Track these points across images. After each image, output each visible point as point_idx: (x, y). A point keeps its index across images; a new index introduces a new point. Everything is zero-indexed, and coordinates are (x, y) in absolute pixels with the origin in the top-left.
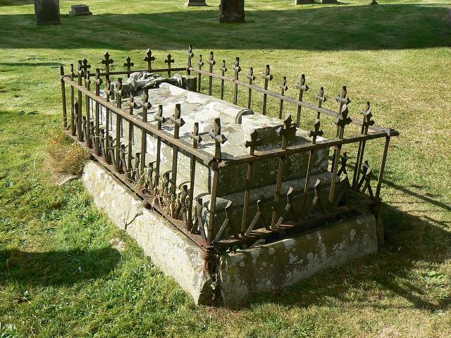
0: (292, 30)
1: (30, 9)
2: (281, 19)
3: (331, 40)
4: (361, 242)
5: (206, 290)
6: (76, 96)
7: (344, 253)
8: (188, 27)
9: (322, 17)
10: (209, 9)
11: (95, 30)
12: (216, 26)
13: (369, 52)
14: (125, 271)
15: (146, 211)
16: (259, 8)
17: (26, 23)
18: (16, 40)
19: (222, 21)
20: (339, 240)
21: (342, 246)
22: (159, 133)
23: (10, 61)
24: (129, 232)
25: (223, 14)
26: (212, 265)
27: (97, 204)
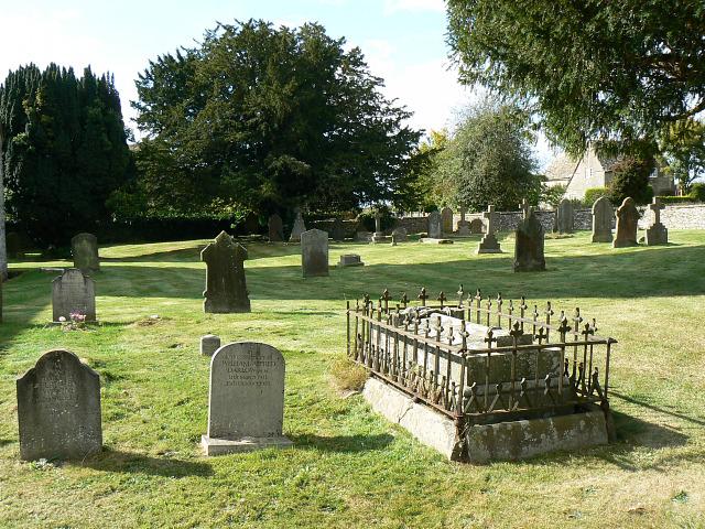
0: (600, 277)
1: (296, 260)
2: (591, 265)
3: (643, 287)
4: (590, 432)
5: (456, 449)
6: (360, 326)
7: (576, 440)
8: (475, 277)
9: (639, 262)
10: (503, 256)
11: (368, 282)
12: (510, 275)
13: (684, 298)
14: (397, 446)
15: (417, 406)
16: (566, 254)
17: (291, 275)
18: (283, 292)
19: (517, 269)
20: (570, 428)
21: (572, 433)
22: (436, 406)
23: (281, 310)
24: (401, 424)
25: (518, 260)
26: (461, 433)
27: (376, 410)
